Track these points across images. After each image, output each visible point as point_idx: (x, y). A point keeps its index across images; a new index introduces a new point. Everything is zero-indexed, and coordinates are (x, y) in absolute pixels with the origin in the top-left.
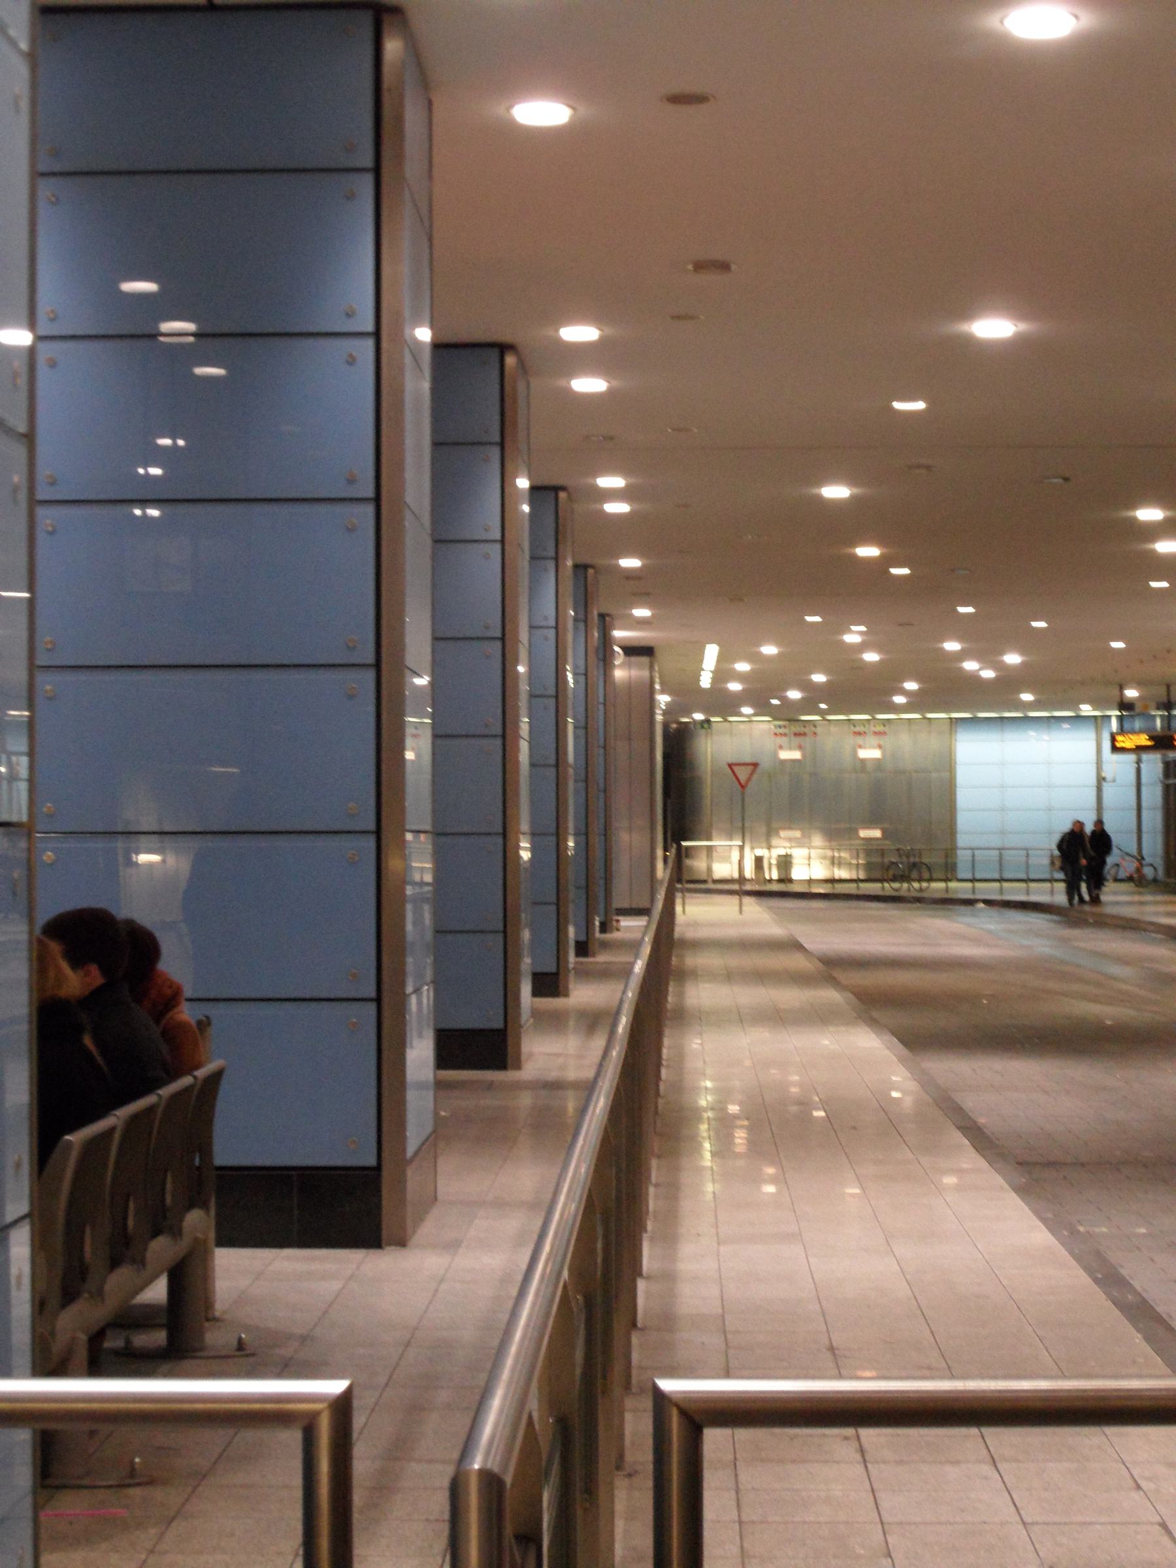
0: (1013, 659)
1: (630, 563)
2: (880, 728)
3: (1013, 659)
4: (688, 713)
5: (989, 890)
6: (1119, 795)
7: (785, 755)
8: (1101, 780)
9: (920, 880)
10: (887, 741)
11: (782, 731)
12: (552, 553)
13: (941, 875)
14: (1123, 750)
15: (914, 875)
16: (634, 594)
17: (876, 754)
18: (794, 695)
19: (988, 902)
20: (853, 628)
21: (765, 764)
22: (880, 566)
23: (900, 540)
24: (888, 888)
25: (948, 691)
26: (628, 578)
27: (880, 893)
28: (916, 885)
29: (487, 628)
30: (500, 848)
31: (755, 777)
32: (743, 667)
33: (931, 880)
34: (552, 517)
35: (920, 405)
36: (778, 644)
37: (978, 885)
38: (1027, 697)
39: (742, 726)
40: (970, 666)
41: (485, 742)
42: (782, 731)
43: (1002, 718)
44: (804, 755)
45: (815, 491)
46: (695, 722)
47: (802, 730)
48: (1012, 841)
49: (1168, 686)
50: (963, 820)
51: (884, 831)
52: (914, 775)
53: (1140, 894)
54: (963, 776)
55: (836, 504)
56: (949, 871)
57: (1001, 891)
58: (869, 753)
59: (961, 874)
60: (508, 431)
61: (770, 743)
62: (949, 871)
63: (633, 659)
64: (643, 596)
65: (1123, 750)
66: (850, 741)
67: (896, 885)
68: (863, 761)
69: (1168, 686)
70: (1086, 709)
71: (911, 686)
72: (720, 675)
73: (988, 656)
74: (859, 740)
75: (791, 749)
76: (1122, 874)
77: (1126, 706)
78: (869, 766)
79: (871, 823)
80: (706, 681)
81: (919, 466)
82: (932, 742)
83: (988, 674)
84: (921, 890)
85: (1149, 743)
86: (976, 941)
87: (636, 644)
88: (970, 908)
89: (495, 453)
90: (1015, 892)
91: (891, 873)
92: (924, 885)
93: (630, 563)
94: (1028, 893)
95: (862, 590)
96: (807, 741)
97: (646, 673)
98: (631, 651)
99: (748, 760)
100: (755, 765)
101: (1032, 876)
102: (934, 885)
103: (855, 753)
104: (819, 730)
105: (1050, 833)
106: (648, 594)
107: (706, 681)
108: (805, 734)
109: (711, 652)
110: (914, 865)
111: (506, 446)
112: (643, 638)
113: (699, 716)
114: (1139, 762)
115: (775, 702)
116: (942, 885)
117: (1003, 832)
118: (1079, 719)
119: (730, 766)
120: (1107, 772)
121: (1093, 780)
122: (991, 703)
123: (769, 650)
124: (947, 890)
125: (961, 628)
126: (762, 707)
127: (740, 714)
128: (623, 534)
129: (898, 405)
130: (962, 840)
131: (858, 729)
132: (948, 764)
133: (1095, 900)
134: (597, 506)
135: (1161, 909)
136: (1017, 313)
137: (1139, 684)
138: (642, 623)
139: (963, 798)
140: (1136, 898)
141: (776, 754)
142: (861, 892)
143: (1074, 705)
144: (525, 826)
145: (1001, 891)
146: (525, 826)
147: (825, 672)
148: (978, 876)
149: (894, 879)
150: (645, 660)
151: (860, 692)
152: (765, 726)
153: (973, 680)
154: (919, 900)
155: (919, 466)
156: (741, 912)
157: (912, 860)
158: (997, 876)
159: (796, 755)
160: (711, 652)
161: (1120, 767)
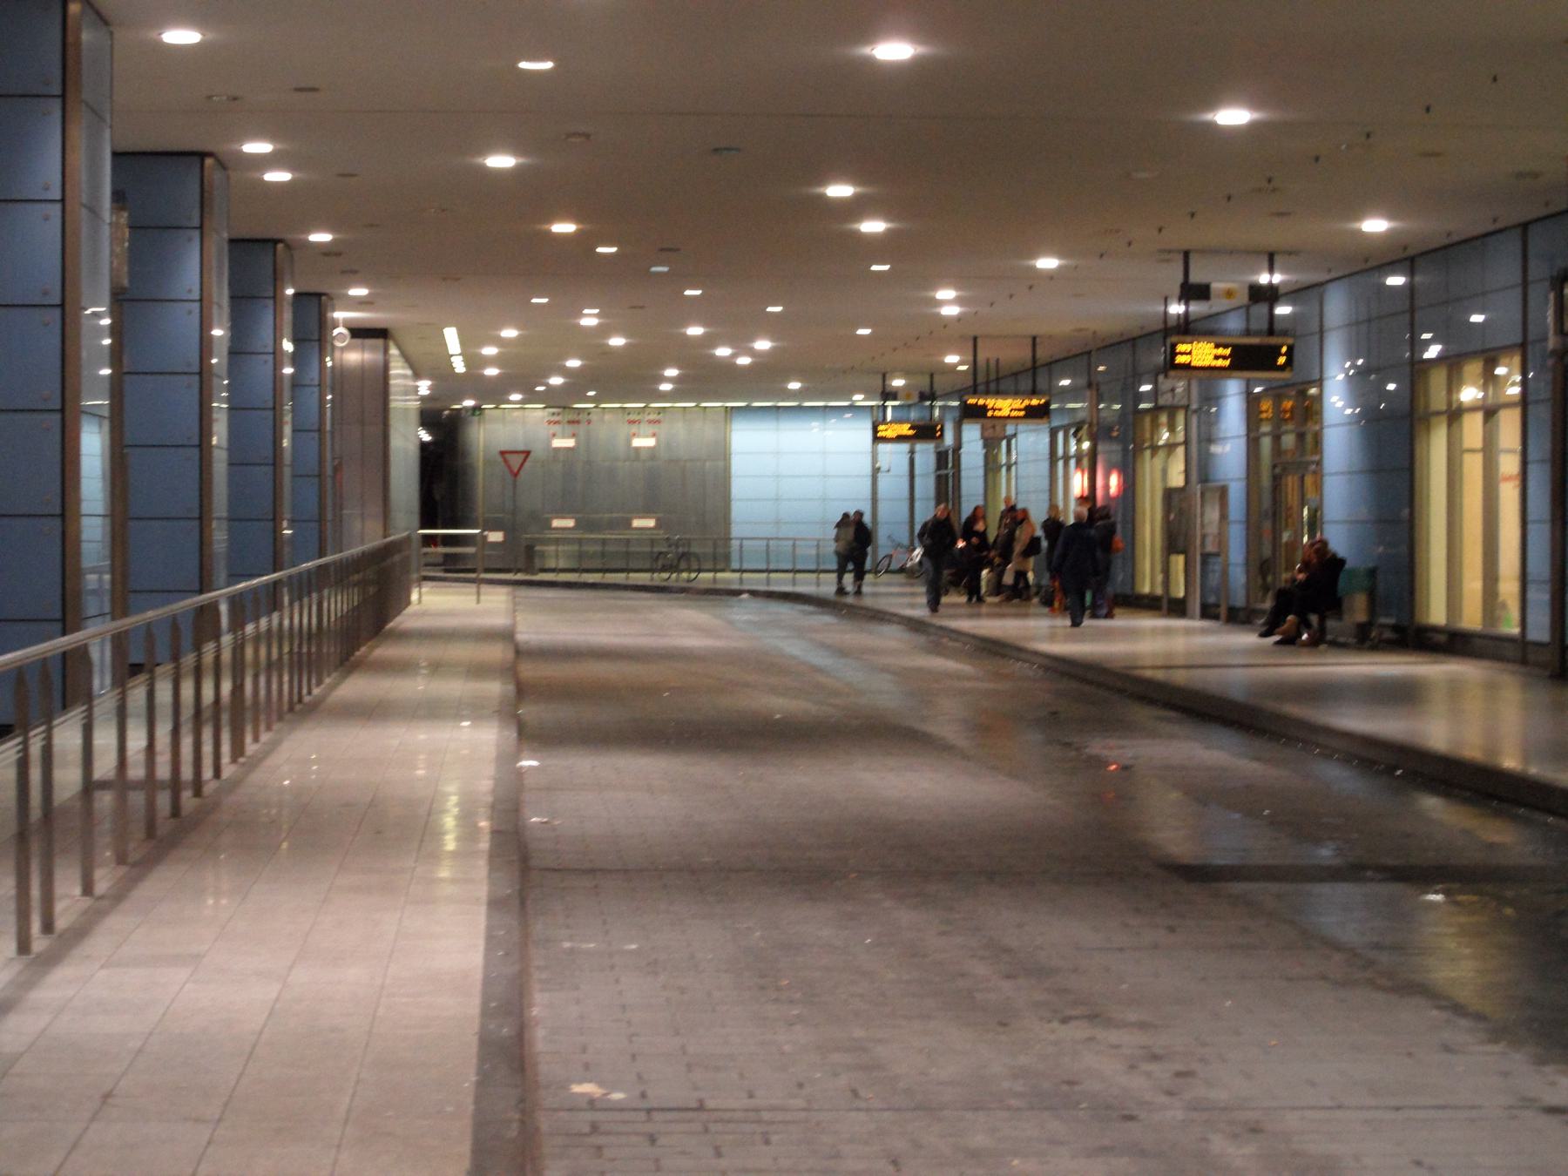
0: (763, 345)
1: (321, 237)
2: (652, 417)
3: (763, 345)
4: (459, 401)
5: (756, 581)
6: (893, 486)
7: (558, 443)
8: (876, 471)
9: (690, 571)
10: (663, 429)
11: (556, 418)
12: (196, 222)
13: (709, 565)
14: (885, 440)
15: (683, 565)
16: (343, 272)
17: (650, 442)
18: (556, 381)
19: (754, 593)
20: (586, 311)
21: (538, 451)
22: (583, 242)
23: (598, 221)
24: (660, 578)
25: (706, 379)
26: (326, 254)
27: (648, 583)
28: (685, 575)
29: (45, 293)
30: (58, 533)
31: (527, 464)
32: (490, 351)
33: (699, 571)
34: (198, 181)
35: (548, 65)
36: (517, 327)
37: (745, 575)
38: (794, 386)
39: (516, 414)
40: (723, 352)
41: (46, 416)
42: (556, 418)
43: (800, 408)
44: (577, 442)
45: (480, 160)
46: (465, 408)
47: (575, 417)
48: (785, 531)
49: (932, 376)
50: (738, 510)
51: (658, 520)
52: (688, 465)
53: (912, 585)
54: (738, 465)
55: (499, 174)
56: (720, 560)
57: (768, 582)
58: (644, 442)
59: (735, 565)
60: (69, 83)
61: (544, 430)
62: (720, 560)
63: (358, 341)
64: (353, 274)
65: (885, 440)
66: (624, 429)
67: (665, 575)
68: (637, 449)
69: (932, 376)
70: (858, 398)
71: (672, 372)
72: (474, 362)
73: (742, 346)
74: (634, 429)
75: (563, 437)
76: (894, 566)
77: (888, 395)
78: (643, 455)
79: (645, 513)
80: (459, 366)
81: (575, 134)
82: (707, 431)
83: (744, 361)
84: (689, 581)
85: (911, 432)
86: (616, 635)
87: (368, 325)
88: (735, 599)
89: (56, 106)
90: (782, 583)
91: (660, 563)
92: (693, 575)
93: (321, 237)
94: (794, 582)
95: (570, 270)
96: (581, 429)
97: (379, 357)
98: (359, 333)
99: (521, 448)
100: (527, 453)
101: (799, 567)
102: (702, 575)
103: (629, 442)
104: (593, 417)
105: (824, 523)
106: (355, 272)
107: (459, 366)
108: (578, 422)
109: (451, 336)
110: (683, 554)
111: (68, 95)
112: (369, 320)
113: (469, 403)
114: (912, 452)
115: (540, 389)
116: (710, 575)
117: (777, 523)
118: (852, 408)
119: (503, 453)
120: (883, 463)
121: (868, 470)
122: (758, 388)
123: (510, 333)
124: (715, 580)
125: (694, 311)
126: (531, 397)
127: (509, 402)
128: (299, 204)
129: (524, 65)
130: (736, 531)
131: (633, 417)
132: (723, 454)
133: (858, 592)
134: (257, 175)
135: (906, 600)
136: (1253, 104)
137: (906, 373)
138: (360, 303)
139: (738, 488)
140: (908, 589)
141: (549, 443)
142: (631, 582)
143: (847, 393)
144: (287, 515)
145: (768, 582)
146: (287, 515)
147: (580, 358)
148: (745, 566)
149: (663, 569)
150: (380, 342)
151: (624, 379)
152: (540, 414)
153: (727, 367)
154: (683, 590)
155: (575, 134)
156: (478, 601)
157: (681, 550)
158: (764, 567)
159: (570, 443)
160: (451, 336)
161: (894, 456)
